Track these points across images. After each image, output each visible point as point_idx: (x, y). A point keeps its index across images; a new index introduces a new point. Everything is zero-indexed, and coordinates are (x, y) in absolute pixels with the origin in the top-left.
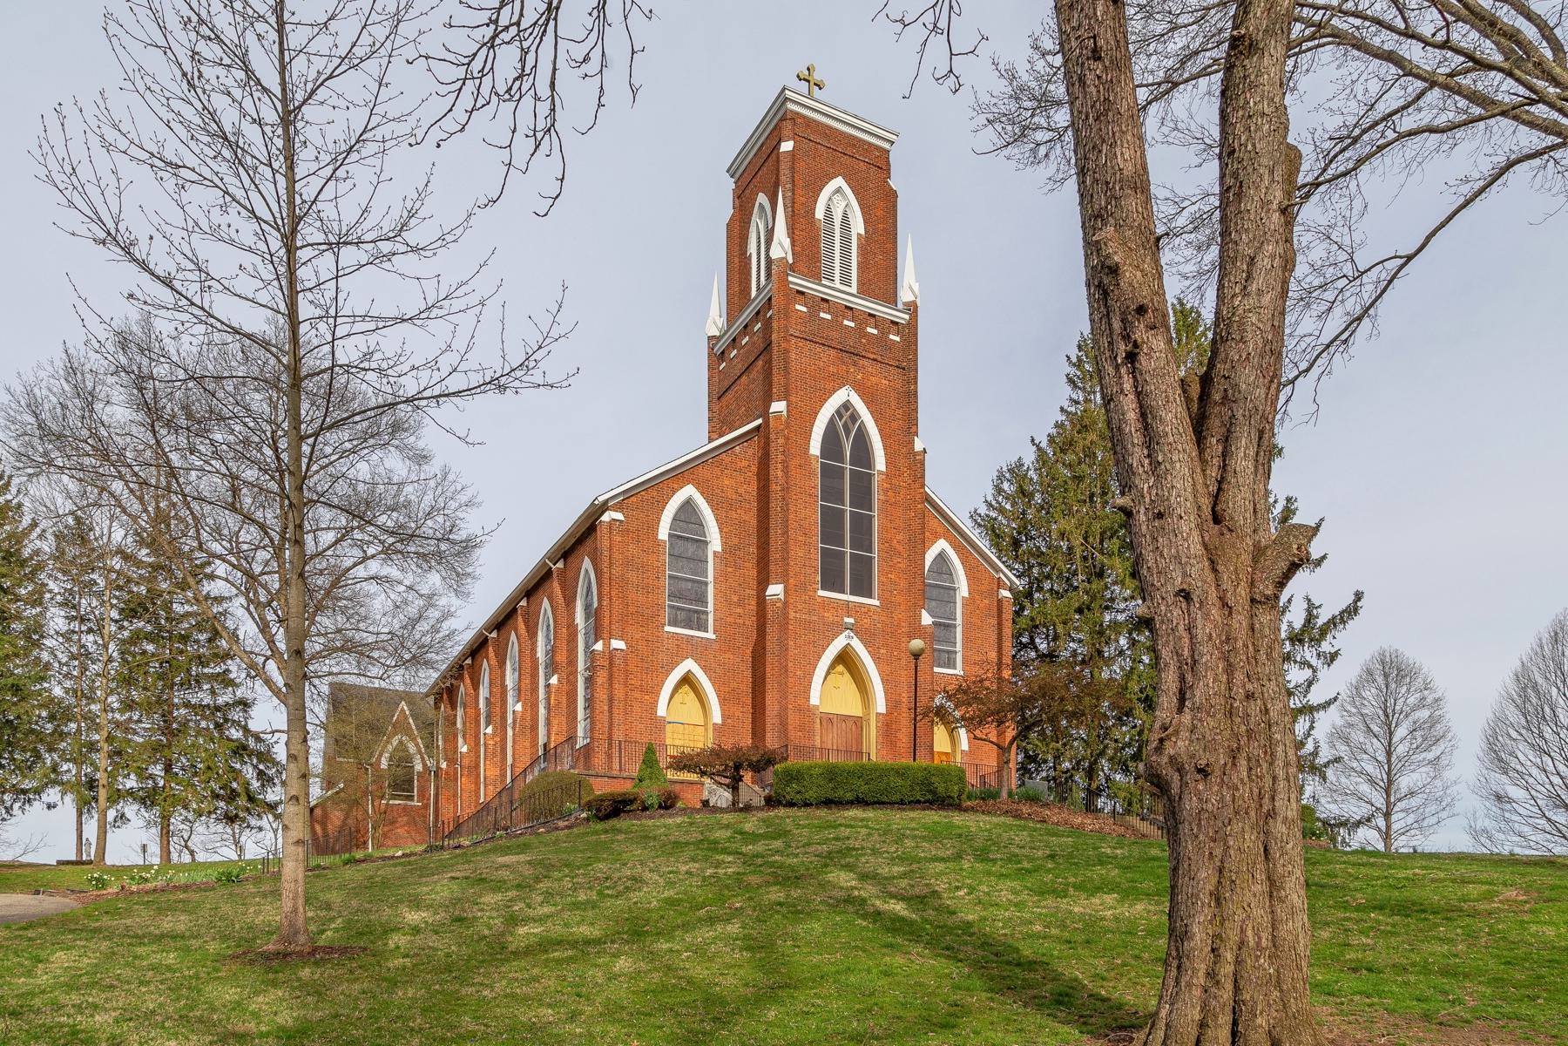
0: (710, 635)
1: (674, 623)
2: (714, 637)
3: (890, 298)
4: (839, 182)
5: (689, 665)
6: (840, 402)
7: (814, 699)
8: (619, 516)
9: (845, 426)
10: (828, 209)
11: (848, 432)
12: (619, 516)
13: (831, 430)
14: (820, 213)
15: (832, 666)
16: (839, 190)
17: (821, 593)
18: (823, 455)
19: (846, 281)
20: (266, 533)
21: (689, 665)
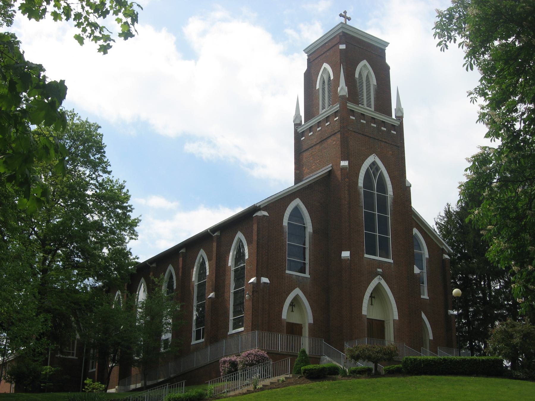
0: (307, 275)
2: (309, 276)
3: (389, 113)
4: (365, 62)
5: (297, 291)
6: (371, 162)
7: (364, 312)
8: (266, 213)
10: (360, 74)
12: (266, 213)
14: (357, 76)
15: (372, 297)
16: (365, 66)
17: (366, 256)
18: (364, 187)
19: (369, 105)
21: (297, 291)
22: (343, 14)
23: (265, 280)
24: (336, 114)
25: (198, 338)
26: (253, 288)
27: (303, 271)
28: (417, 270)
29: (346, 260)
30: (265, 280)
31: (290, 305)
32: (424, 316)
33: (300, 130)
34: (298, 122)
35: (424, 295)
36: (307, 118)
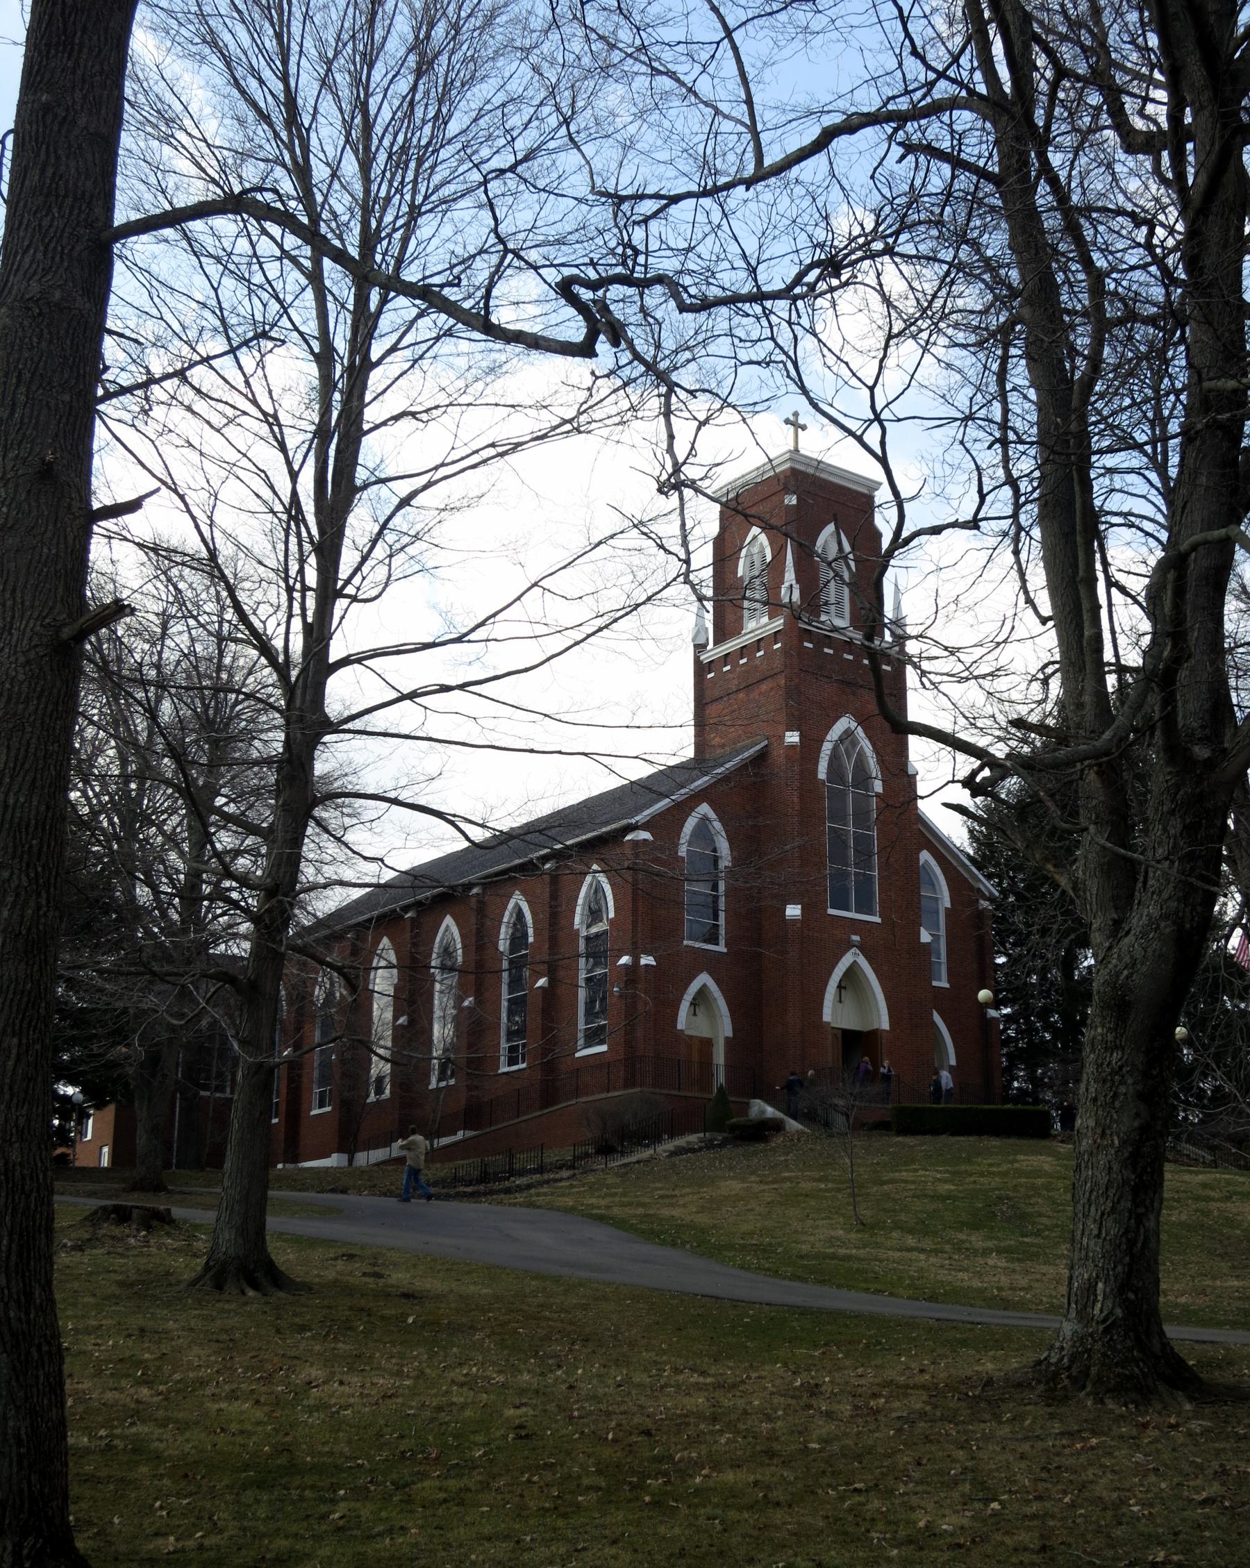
0: (721, 948)
1: (690, 939)
2: (725, 950)
5: (704, 979)
7: (827, 1016)
9: (846, 751)
11: (849, 757)
13: (834, 757)
15: (840, 987)
17: (831, 911)
20: (463, 262)
21: (704, 979)
22: (792, 418)
23: (647, 960)
24: (776, 636)
25: (512, 1061)
26: (627, 974)
27: (714, 939)
28: (925, 937)
29: (794, 922)
30: (647, 960)
31: (691, 1004)
32: (937, 1018)
33: (706, 658)
34: (701, 641)
35: (940, 980)
36: (720, 637)
